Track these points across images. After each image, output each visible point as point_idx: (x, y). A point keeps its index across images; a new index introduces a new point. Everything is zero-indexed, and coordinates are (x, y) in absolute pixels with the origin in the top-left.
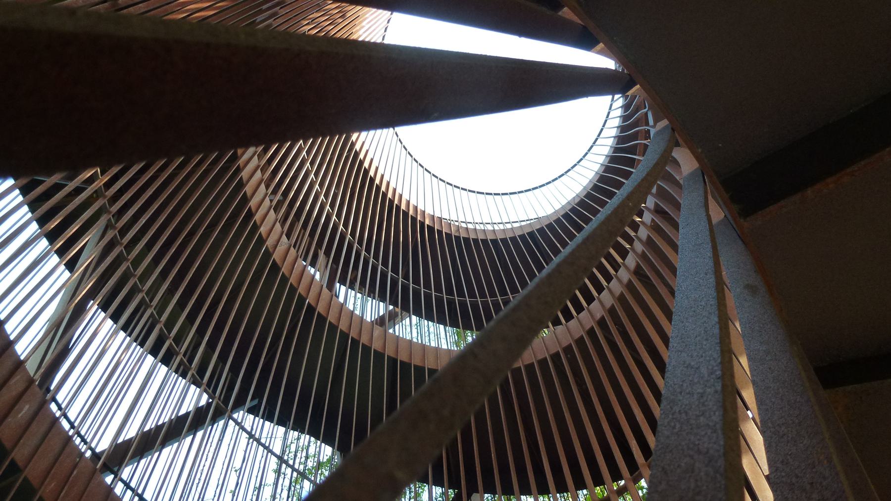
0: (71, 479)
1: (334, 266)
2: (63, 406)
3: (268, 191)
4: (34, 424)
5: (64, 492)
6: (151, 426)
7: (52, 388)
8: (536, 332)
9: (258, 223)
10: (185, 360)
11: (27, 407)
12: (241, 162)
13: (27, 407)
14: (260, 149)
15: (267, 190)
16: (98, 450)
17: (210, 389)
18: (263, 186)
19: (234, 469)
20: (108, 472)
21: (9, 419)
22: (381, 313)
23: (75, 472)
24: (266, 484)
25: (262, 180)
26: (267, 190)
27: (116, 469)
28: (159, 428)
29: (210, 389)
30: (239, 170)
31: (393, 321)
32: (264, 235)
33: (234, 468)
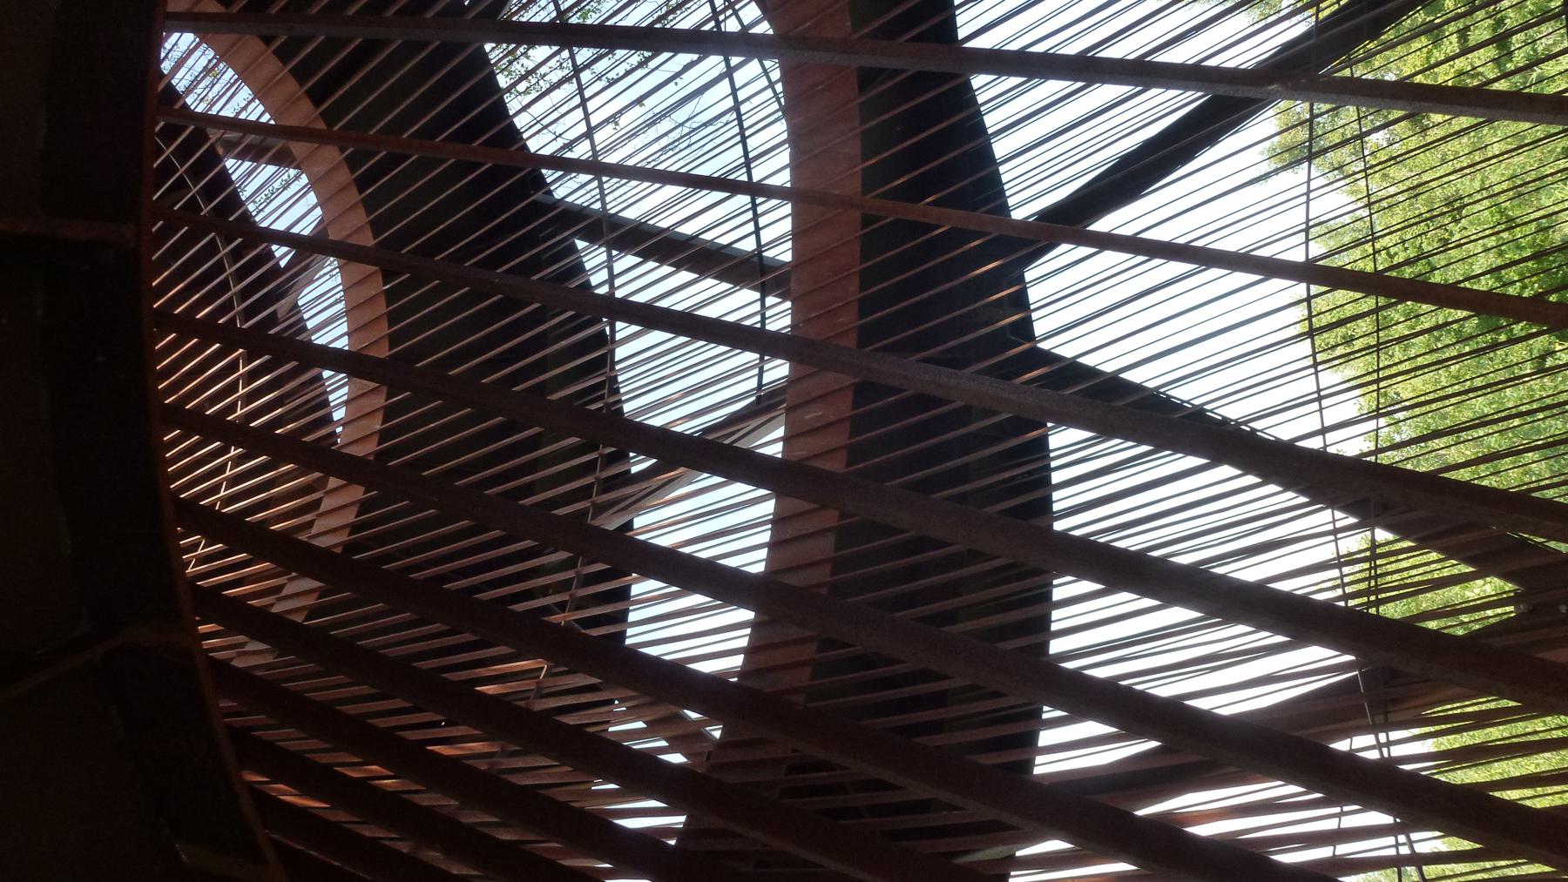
0: (822, 312)
1: (207, 404)
2: (756, 371)
3: (282, 582)
4: (814, 394)
5: (837, 305)
6: (639, 163)
7: (754, 398)
8: (1271, 83)
9: (376, 439)
10: (606, 391)
11: (808, 417)
12: (343, 537)
13: (808, 417)
14: (303, 537)
15: (321, 499)
16: (757, 295)
17: (604, 394)
18: (323, 508)
19: (617, 127)
20: (765, 262)
21: (832, 418)
22: (271, 169)
23: (814, 315)
24: (594, 75)
25: (327, 493)
26: (321, 499)
27: (755, 259)
28: (679, 266)
29: (604, 394)
30: (355, 528)
31: (264, 144)
32: (380, 416)
33: (615, 129)
